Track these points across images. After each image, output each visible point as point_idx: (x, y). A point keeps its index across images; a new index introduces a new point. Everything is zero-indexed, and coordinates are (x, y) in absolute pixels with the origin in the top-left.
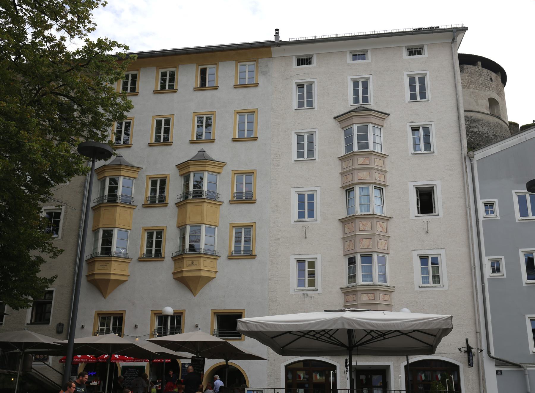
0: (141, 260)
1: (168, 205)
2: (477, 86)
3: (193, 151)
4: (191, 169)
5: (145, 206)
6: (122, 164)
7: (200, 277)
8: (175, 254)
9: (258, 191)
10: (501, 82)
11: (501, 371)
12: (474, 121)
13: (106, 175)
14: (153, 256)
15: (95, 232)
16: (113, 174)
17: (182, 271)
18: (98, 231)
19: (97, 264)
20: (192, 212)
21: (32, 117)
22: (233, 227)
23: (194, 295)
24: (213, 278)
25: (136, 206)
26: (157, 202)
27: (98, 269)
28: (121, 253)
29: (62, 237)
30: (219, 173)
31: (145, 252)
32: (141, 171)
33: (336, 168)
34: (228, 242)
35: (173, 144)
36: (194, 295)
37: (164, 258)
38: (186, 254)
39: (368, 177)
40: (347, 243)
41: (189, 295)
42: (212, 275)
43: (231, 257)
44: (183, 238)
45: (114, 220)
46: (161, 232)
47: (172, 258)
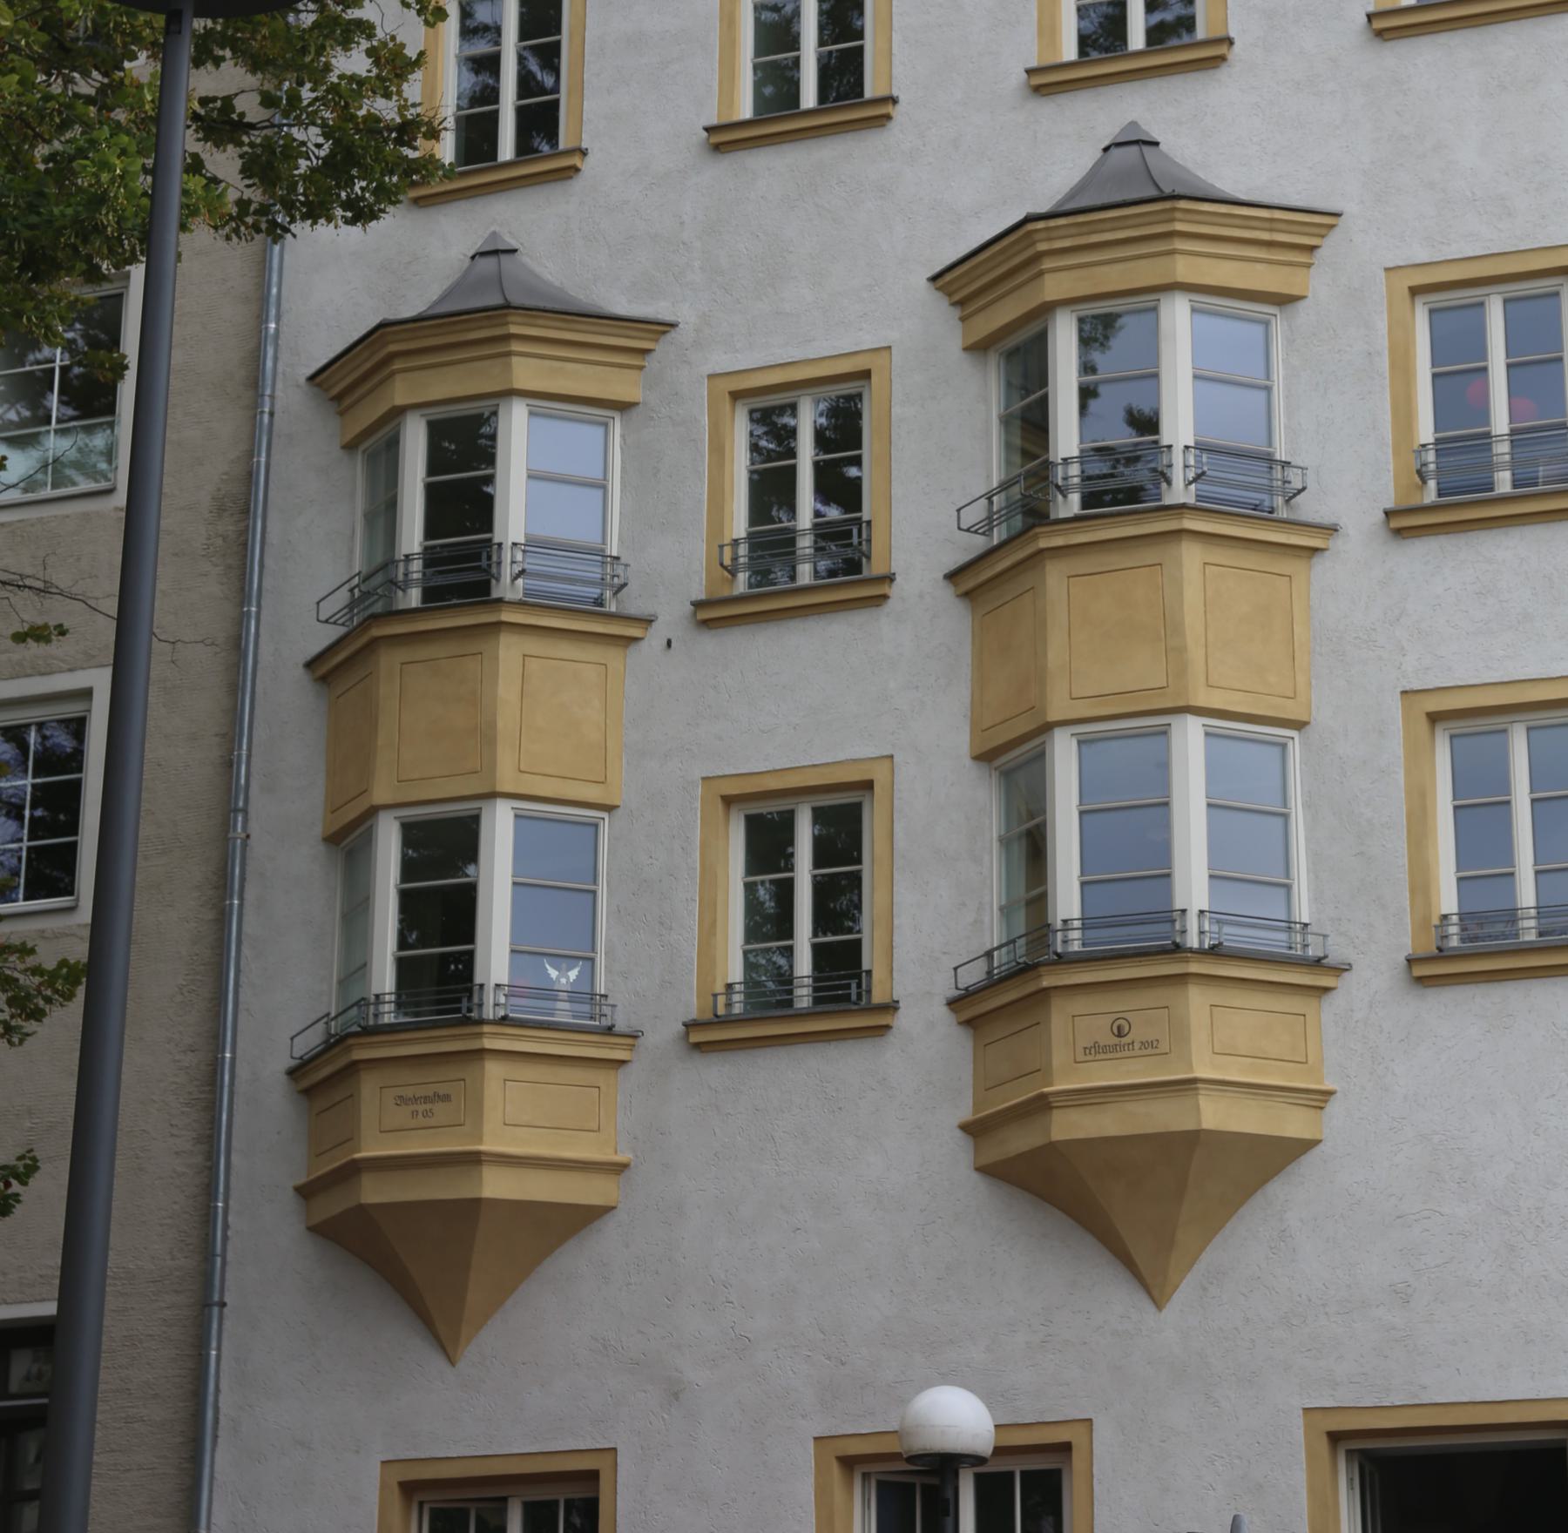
0: (708, 1036)
1: (894, 591)
3: (1058, 154)
4: (1054, 286)
5: (713, 614)
6: (516, 299)
7: (1194, 1139)
8: (973, 975)
13: (399, 400)
14: (803, 997)
15: (348, 841)
16: (449, 384)
17: (1041, 1105)
18: (368, 840)
19: (369, 1088)
20: (1084, 622)
21: (237, 30)
22: (1434, 718)
23: (1159, 1305)
24: (1305, 1146)
25: (647, 621)
27: (385, 1127)
28: (548, 993)
30: (1283, 300)
32: (663, 349)
34: (1400, 845)
35: (897, 112)
37: (891, 1007)
38: (1063, 960)
41: (1112, 1300)
42: (1291, 1123)
43: (1437, 967)
44: (1031, 847)
45: (485, 736)
46: (857, 808)
47: (952, 1003)
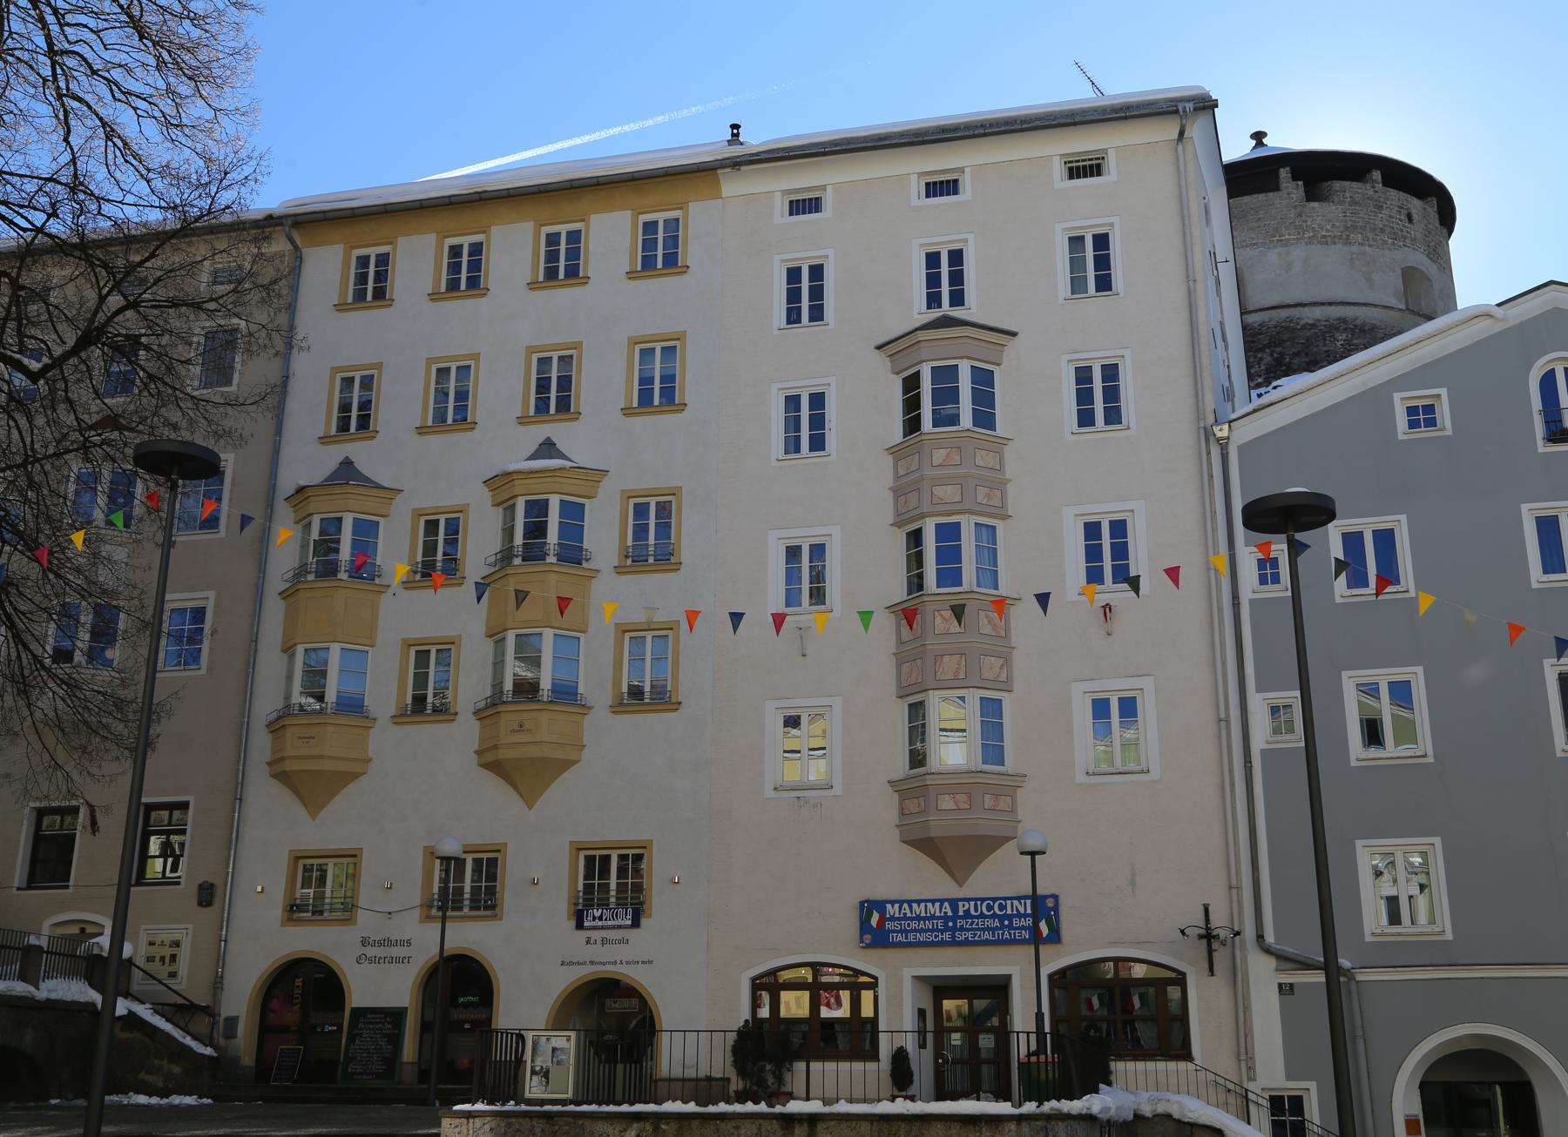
2: (1371, 236)
9: (684, 542)
10: (1437, 223)
11: (1291, 985)
12: (1363, 331)
19: (289, 733)
23: (530, 807)
26: (651, 560)
29: (210, 669)
31: (409, 700)
33: (881, 474)
36: (530, 807)
39: (958, 498)
40: (906, 667)
